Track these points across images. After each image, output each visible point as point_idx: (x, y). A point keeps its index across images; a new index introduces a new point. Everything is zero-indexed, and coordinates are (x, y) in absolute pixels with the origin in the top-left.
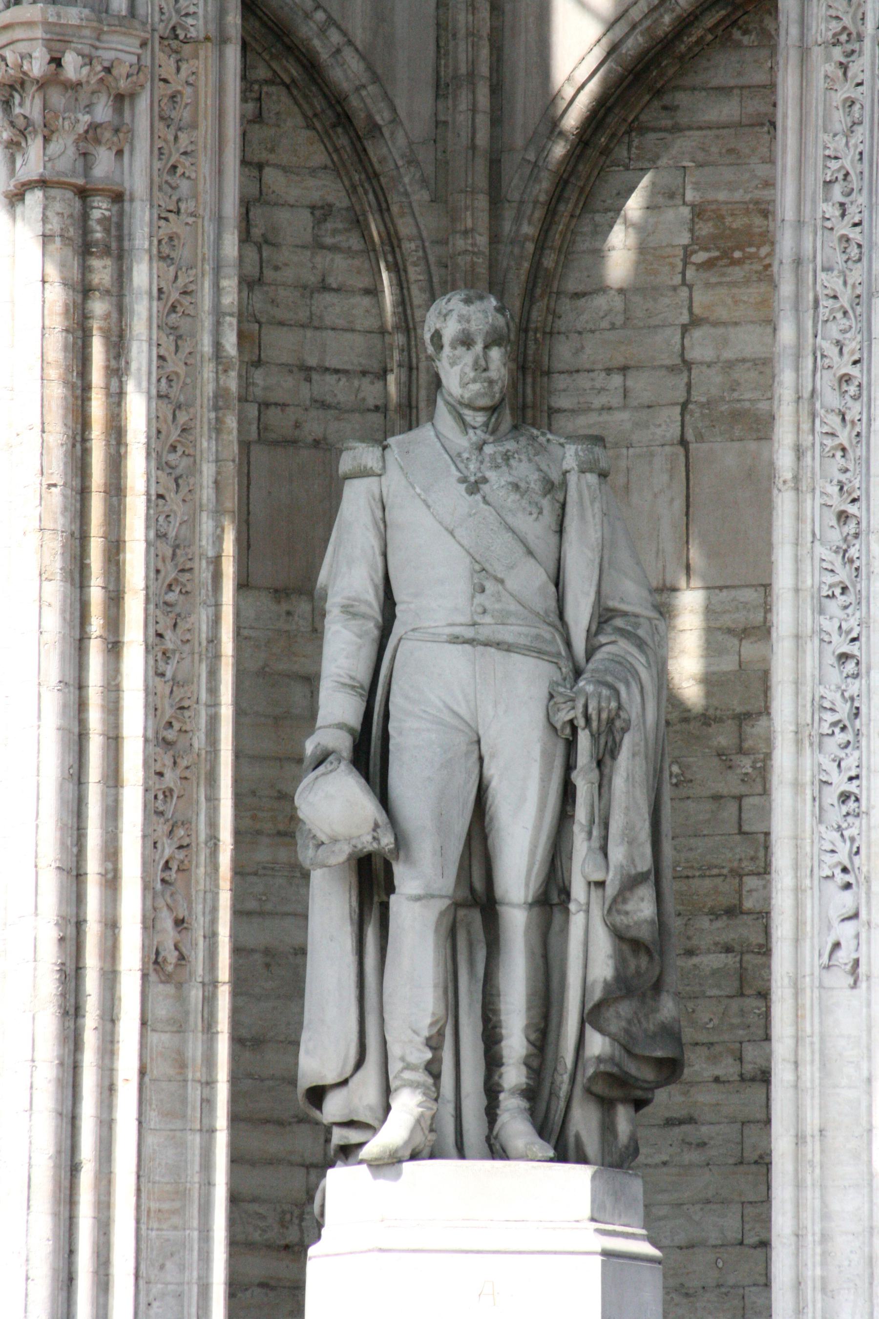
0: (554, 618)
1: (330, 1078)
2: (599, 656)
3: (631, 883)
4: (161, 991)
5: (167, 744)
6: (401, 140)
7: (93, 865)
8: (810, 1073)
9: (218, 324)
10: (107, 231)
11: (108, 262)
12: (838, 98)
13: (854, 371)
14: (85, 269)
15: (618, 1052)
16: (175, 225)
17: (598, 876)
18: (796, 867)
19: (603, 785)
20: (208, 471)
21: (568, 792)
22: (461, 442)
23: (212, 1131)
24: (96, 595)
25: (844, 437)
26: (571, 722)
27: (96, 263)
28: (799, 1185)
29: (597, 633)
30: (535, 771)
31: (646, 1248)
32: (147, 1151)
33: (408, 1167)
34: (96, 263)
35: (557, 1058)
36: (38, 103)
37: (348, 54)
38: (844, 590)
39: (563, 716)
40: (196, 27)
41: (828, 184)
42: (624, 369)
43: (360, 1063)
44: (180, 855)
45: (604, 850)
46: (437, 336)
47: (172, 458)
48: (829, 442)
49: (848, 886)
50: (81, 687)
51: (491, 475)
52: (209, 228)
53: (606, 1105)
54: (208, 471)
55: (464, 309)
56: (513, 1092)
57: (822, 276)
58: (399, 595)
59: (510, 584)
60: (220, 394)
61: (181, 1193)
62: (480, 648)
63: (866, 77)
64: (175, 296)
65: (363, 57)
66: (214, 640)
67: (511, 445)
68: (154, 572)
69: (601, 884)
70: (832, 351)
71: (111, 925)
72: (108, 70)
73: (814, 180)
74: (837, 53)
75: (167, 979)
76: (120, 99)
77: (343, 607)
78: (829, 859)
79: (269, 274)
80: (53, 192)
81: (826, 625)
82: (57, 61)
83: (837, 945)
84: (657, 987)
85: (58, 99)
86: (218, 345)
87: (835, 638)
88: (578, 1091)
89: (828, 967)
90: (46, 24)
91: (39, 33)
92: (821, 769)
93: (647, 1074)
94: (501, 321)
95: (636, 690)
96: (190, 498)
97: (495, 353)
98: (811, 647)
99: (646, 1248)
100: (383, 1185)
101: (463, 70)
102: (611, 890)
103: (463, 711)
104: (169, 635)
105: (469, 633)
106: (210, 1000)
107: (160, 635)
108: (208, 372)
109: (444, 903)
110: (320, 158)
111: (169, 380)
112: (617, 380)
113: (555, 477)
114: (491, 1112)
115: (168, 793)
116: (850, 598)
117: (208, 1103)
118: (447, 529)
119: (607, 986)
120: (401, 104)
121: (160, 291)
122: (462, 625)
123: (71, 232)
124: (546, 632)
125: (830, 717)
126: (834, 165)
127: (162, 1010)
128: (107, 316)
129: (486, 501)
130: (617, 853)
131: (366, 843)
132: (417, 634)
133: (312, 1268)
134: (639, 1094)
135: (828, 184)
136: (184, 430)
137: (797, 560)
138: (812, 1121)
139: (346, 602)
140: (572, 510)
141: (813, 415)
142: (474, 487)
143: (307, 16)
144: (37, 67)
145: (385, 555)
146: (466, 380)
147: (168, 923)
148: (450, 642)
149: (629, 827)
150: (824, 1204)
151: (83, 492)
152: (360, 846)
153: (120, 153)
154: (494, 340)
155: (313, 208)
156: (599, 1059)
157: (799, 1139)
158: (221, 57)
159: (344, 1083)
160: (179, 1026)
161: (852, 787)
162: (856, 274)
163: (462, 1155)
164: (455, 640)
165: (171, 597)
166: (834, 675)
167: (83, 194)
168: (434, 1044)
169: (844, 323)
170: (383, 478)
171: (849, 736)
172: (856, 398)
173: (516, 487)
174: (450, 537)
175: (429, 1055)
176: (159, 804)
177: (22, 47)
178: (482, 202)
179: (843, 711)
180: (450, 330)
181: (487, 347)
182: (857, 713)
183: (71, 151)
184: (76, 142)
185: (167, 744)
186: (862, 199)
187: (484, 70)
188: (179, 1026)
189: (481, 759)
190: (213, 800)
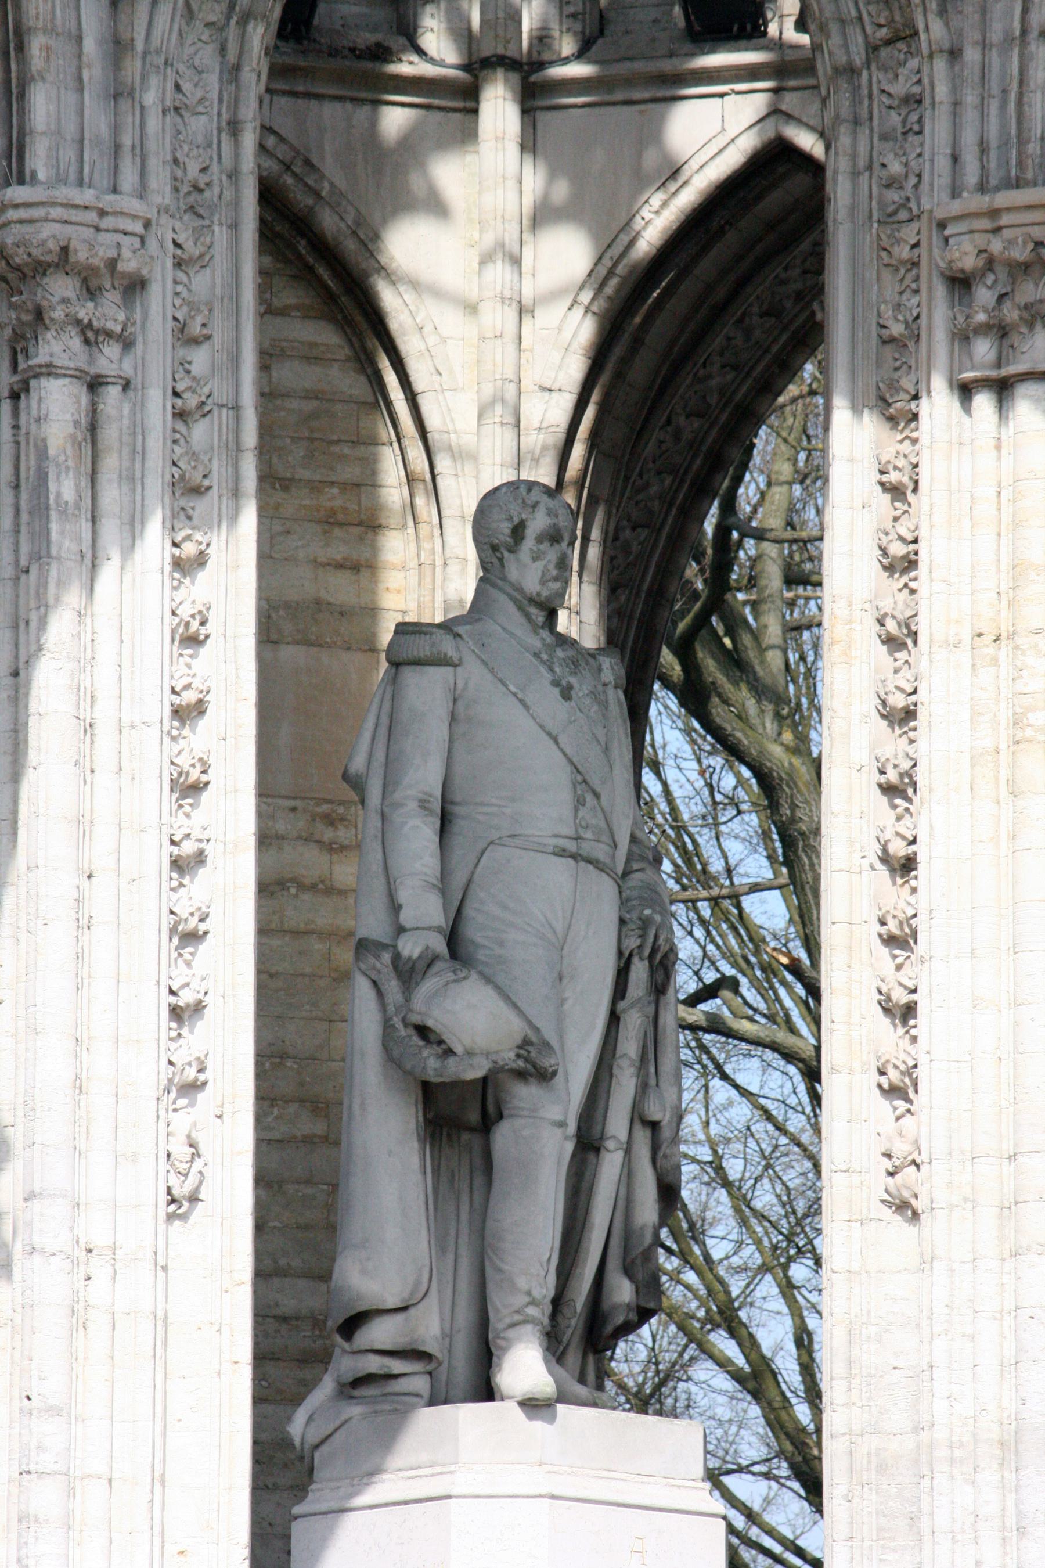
62: (582, 864)
77: (421, 801)
105: (571, 846)
118: (549, 734)
122: (566, 837)
132: (516, 841)
139: (421, 796)
142: (566, 693)
146: (548, 577)
148: (555, 854)
152: (501, 1063)
164: (561, 853)
170: (459, 669)
174: (551, 743)
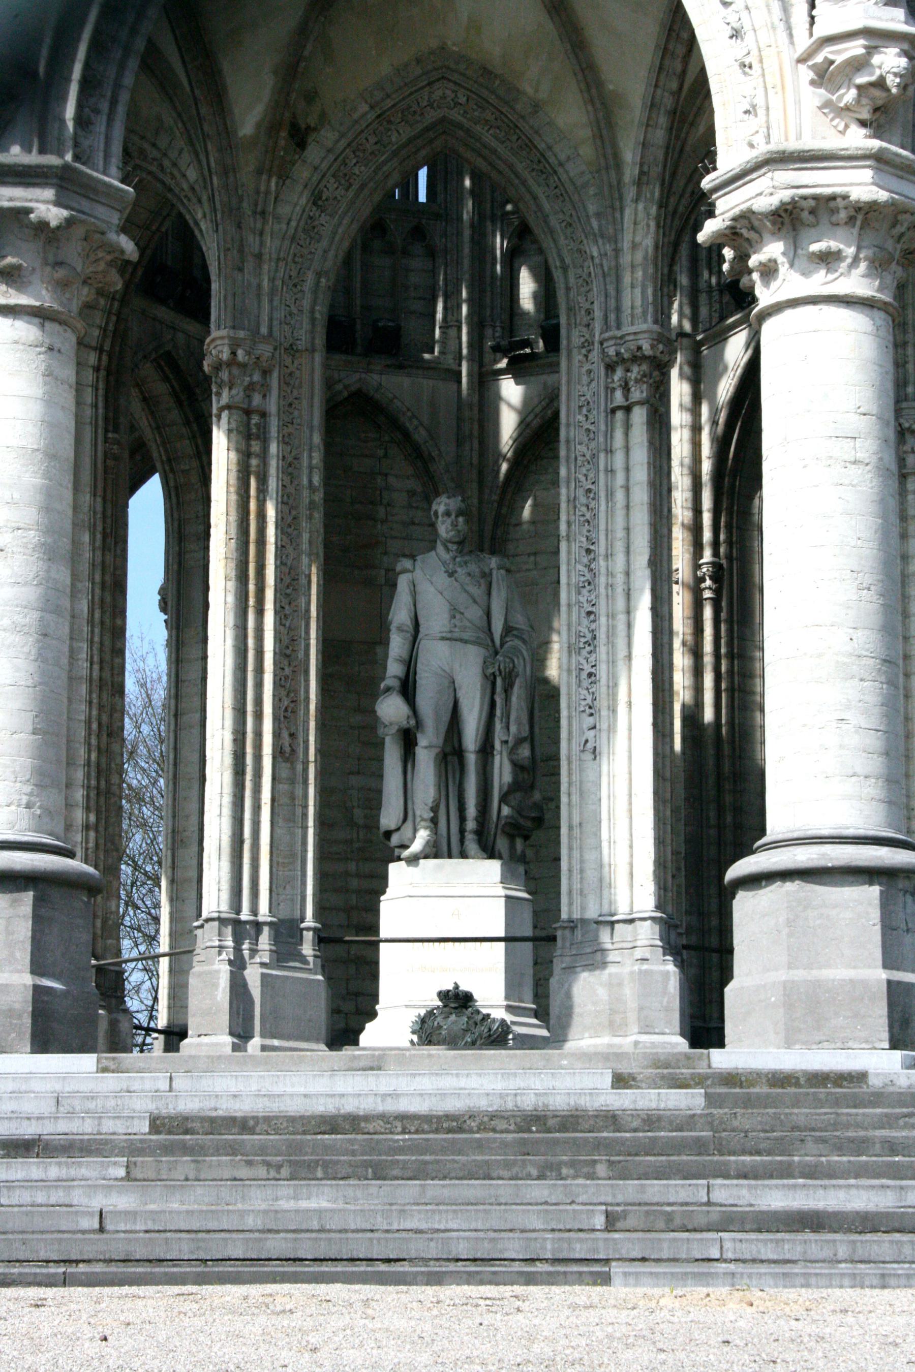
0: (486, 630)
1: (393, 826)
2: (506, 646)
3: (519, 741)
4: (284, 766)
5: (287, 656)
6: (443, 463)
7: (250, 708)
8: (575, 798)
9: (311, 472)
10: (259, 429)
11: (258, 442)
12: (584, 370)
13: (592, 487)
14: (249, 446)
15: (516, 815)
16: (291, 429)
17: (505, 738)
18: (569, 707)
19: (507, 700)
20: (305, 537)
21: (493, 705)
22: (446, 556)
23: (307, 827)
24: (252, 587)
25: (588, 516)
26: (493, 674)
27: (253, 443)
28: (570, 849)
29: (506, 635)
30: (478, 695)
31: (525, 895)
32: (275, 836)
33: (422, 861)
34: (253, 443)
35: (490, 817)
36: (227, 374)
37: (421, 429)
38: (589, 584)
39: (490, 671)
40: (301, 345)
41: (580, 407)
42: (535, 554)
43: (405, 819)
44: (292, 705)
45: (508, 729)
46: (436, 513)
47: (289, 530)
48: (582, 519)
49: (591, 715)
50: (245, 628)
51: (459, 570)
52: (307, 431)
53: (512, 838)
54: (305, 537)
55: (447, 501)
56: (470, 832)
57: (578, 447)
58: (421, 621)
59: (467, 615)
60: (312, 503)
61: (293, 855)
63: (595, 359)
64: (290, 459)
65: (427, 430)
66: (308, 611)
67: (467, 558)
68: (279, 580)
69: (506, 742)
70: (583, 479)
71: (258, 734)
72: (258, 358)
73: (574, 405)
74: (584, 351)
75: (287, 760)
76: (266, 373)
78: (583, 703)
79: (390, 518)
80: (234, 411)
81: (581, 599)
82: (234, 353)
83: (587, 741)
84: (532, 787)
85: (236, 371)
86: (310, 482)
87: (585, 605)
88: (499, 832)
89: (583, 751)
90: (230, 338)
91: (226, 341)
92: (580, 664)
93: (529, 824)
94: (463, 505)
95: (521, 661)
96: (297, 548)
97: (461, 519)
98: (575, 609)
99: (525, 895)
100: (411, 869)
101: (467, 433)
102: (510, 744)
103: (447, 668)
104: (287, 607)
105: (449, 635)
106: (306, 770)
107: (283, 608)
108: (306, 493)
109: (437, 750)
110: (410, 471)
111: (288, 497)
112: (532, 558)
113: (487, 570)
114: (462, 841)
115: (286, 677)
116: (592, 587)
117: (305, 815)
119: (509, 785)
120: (443, 448)
121: (284, 457)
123: (241, 429)
124: (482, 635)
125: (583, 640)
126: (583, 399)
127: (284, 773)
128: (258, 466)
129: (456, 580)
130: (513, 728)
131: (404, 724)
133: (383, 906)
134: (526, 832)
135: (580, 407)
136: (294, 518)
137: (568, 571)
138: (576, 820)
140: (494, 585)
141: (575, 507)
142: (451, 574)
143: (404, 414)
144: (225, 356)
145: (415, 605)
147: (285, 734)
149: (518, 717)
150: (581, 856)
151: (246, 543)
153: (264, 396)
154: (460, 513)
155: (408, 491)
156: (507, 817)
157: (571, 828)
158: (313, 358)
159: (398, 829)
160: (292, 781)
161: (593, 670)
162: (593, 445)
163: (450, 856)
164: (443, 639)
165: (288, 591)
166: (585, 622)
167: (248, 412)
168: (435, 809)
169: (588, 467)
171: (591, 648)
172: (593, 499)
173: (469, 574)
175: (432, 815)
176: (283, 682)
177: (219, 348)
178: (475, 485)
179: (589, 636)
180: (441, 509)
181: (457, 516)
182: (594, 638)
183: (242, 394)
184: (245, 391)
185: (287, 656)
186: (595, 412)
187: (476, 434)
188: (292, 781)
189: (455, 690)
190: (307, 681)
